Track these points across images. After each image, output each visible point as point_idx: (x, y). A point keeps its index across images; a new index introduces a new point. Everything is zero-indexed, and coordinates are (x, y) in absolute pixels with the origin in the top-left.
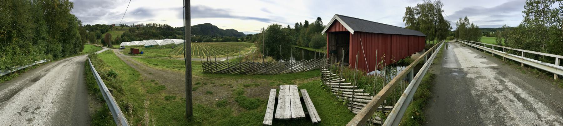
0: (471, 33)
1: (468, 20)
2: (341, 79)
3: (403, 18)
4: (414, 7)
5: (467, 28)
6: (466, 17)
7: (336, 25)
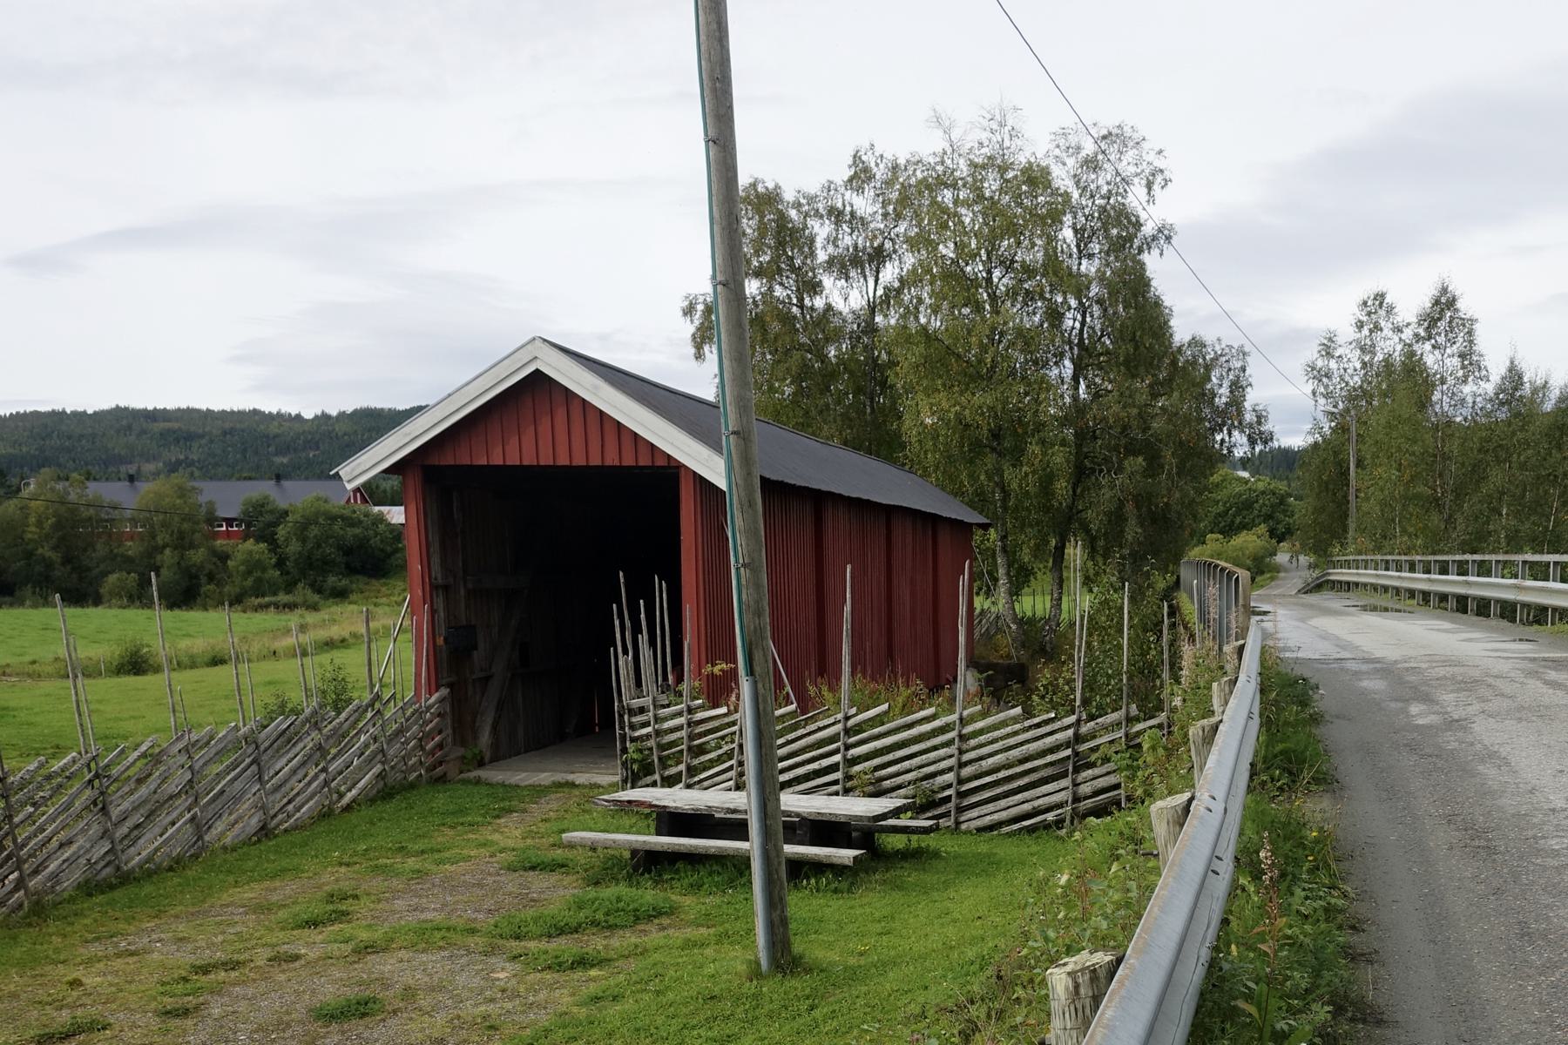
0: (1497, 477)
1: (1467, 327)
2: (847, 718)
3: (689, 311)
4: (813, 188)
5: (385, 491)
6: (1444, 290)
7: (545, 423)
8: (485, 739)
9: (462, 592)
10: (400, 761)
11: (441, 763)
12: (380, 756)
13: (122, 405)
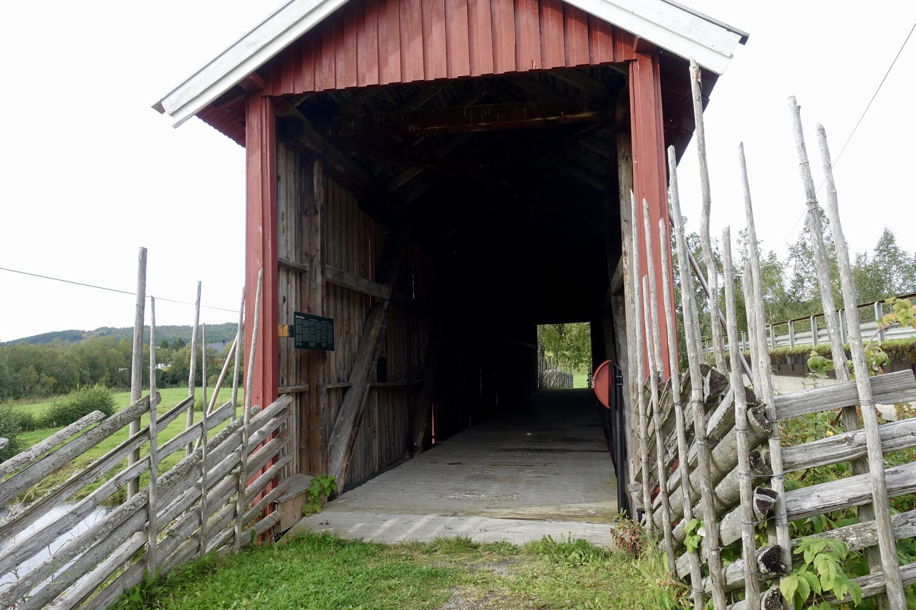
8: (339, 462)
9: (319, 279)
10: (189, 519)
11: (273, 506)
12: (142, 516)
13: (229, 322)
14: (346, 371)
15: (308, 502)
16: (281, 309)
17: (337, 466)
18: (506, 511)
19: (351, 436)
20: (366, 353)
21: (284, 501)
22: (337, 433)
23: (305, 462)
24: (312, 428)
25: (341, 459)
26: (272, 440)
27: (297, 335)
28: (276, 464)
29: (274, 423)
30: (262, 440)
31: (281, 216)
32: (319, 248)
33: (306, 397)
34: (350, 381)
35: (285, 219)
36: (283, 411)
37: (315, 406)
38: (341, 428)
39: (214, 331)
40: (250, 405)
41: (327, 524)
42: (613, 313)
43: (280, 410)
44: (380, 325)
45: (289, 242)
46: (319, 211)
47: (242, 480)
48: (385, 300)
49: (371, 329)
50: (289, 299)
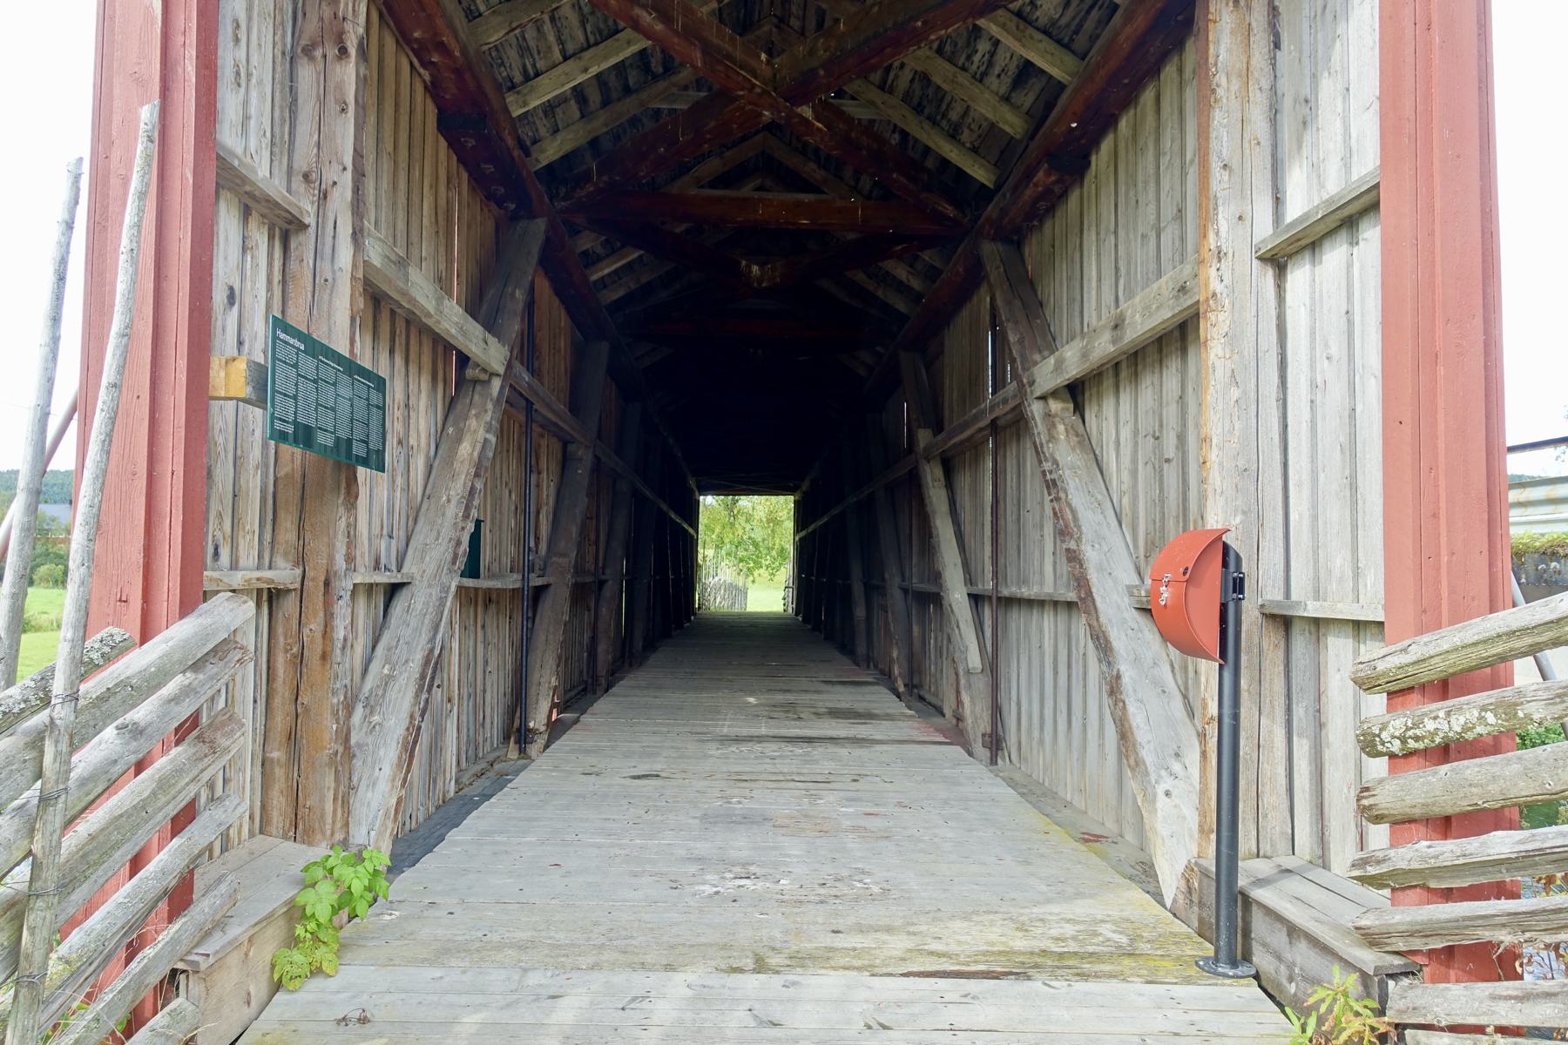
14: (394, 542)
15: (293, 941)
16: (219, 323)
17: (374, 805)
18: (898, 944)
19: (412, 717)
20: (449, 501)
21: (211, 960)
22: (370, 708)
23: (279, 802)
24: (304, 699)
25: (383, 785)
26: (175, 751)
27: (279, 397)
28: (187, 833)
29: (186, 692)
30: (133, 758)
31: (230, 30)
32: (348, 161)
33: (289, 605)
34: (405, 570)
35: (243, 84)
36: (220, 651)
37: (319, 635)
38: (383, 695)
39: (53, 482)
40: (84, 628)
41: (363, 1020)
42: (1044, 438)
43: (210, 646)
44: (481, 434)
45: (252, 122)
46: (353, 51)
47: (32, 930)
48: (493, 374)
49: (459, 440)
50: (248, 300)
